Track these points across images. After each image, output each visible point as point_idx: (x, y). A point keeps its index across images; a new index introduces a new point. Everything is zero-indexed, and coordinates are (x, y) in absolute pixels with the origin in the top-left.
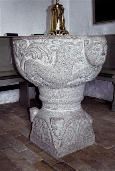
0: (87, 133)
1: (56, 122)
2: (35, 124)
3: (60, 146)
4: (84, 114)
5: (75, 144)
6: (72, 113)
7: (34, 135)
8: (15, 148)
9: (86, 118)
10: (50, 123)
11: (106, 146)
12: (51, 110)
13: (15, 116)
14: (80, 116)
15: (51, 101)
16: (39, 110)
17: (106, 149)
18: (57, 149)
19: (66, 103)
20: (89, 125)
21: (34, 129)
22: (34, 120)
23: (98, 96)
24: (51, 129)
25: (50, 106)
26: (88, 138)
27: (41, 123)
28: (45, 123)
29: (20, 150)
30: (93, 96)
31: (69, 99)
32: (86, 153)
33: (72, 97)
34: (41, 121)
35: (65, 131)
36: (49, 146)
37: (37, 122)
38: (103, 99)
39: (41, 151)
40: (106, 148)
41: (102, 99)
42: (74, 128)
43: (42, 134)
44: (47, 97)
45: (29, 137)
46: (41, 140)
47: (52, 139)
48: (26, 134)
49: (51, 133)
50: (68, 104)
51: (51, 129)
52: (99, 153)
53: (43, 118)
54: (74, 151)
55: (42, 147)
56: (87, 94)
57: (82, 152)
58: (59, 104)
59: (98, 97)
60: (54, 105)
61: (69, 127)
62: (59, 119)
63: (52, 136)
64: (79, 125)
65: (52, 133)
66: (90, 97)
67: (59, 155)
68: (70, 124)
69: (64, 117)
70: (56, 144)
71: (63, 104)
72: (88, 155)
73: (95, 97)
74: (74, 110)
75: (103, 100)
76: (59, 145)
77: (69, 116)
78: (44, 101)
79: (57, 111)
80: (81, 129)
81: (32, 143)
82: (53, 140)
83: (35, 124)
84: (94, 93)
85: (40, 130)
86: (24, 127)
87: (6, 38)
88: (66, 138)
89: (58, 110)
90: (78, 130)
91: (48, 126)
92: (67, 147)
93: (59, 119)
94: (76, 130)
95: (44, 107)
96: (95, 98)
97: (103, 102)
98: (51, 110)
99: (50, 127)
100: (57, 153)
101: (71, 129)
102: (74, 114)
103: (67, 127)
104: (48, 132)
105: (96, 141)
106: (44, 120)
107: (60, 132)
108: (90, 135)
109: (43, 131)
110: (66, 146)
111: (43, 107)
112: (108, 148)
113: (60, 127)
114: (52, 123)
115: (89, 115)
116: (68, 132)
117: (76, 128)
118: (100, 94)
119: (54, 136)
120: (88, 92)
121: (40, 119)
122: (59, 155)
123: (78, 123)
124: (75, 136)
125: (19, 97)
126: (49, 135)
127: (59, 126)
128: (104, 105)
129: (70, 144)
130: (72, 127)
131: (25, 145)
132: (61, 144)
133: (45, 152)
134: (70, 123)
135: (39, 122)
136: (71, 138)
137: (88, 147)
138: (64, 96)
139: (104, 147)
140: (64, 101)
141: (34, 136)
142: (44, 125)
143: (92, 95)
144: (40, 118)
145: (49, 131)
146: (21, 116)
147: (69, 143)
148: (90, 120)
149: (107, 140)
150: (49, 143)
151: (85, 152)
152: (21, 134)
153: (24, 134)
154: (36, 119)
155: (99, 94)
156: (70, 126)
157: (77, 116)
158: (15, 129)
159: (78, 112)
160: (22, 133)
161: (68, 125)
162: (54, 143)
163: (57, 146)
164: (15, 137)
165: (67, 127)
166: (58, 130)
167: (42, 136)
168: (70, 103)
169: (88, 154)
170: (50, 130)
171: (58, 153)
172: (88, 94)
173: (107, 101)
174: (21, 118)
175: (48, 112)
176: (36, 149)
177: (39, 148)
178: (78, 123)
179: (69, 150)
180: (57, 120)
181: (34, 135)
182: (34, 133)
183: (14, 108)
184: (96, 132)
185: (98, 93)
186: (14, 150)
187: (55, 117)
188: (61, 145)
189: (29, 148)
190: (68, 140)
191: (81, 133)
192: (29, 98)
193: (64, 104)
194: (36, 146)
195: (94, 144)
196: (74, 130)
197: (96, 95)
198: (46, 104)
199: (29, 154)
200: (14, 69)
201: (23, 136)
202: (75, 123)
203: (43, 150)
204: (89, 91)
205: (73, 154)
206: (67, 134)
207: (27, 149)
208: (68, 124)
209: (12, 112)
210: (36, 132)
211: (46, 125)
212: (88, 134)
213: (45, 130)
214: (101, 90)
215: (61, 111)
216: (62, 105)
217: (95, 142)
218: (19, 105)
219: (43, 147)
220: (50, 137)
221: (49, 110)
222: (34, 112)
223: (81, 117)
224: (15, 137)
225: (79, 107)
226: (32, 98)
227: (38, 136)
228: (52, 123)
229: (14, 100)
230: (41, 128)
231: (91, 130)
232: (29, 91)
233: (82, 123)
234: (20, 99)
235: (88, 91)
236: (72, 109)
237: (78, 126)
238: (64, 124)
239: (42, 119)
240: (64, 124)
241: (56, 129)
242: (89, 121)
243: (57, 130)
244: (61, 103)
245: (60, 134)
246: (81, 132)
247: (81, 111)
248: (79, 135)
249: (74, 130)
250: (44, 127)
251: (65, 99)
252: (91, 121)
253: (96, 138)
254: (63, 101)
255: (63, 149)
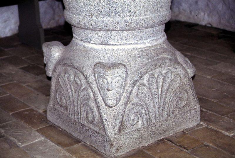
0: (181, 99)
1: (109, 72)
2: (58, 82)
3: (120, 131)
4: (174, 54)
5: (154, 124)
6: (144, 52)
7: (57, 107)
8: (12, 139)
9: (178, 63)
10: (93, 76)
11: (228, 130)
12: (95, 46)
13: (11, 68)
14: (163, 59)
15: (93, 23)
16: (64, 47)
17: (227, 136)
18: (113, 135)
19: (129, 28)
20: (186, 81)
21: (56, 92)
22: (54, 71)
23: (204, 19)
24: (96, 90)
25: (93, 35)
26: (183, 110)
27: (72, 76)
28: (82, 76)
29: (25, 142)
30: (192, 21)
31: (138, 18)
32: (180, 146)
33: (143, 13)
34: (71, 71)
35: (130, 93)
36: (94, 132)
37: (63, 75)
38: (215, 25)
39: (76, 143)
40: (227, 134)
41: (212, 28)
42: (150, 88)
43: (76, 104)
44: (84, 14)
45: (45, 112)
46: (73, 117)
47: (100, 113)
48: (37, 105)
49: (96, 100)
50: (134, 30)
51: (96, 90)
52: (211, 145)
53: (76, 65)
54: (152, 141)
55: (75, 134)
56: (177, 16)
57: (169, 143)
58: (112, 30)
59: (204, 23)
60: (102, 32)
61: (138, 84)
62: (115, 65)
63: (98, 107)
64: (163, 79)
65: (98, 100)
66: (186, 22)
67: (117, 150)
68: (141, 77)
69: (125, 62)
70: (110, 124)
71: (122, 30)
72: (185, 150)
73: (197, 22)
74: (148, 45)
75: (216, 28)
76: (117, 127)
77: (139, 60)
78: (76, 24)
79: (107, 47)
80: (168, 90)
81: (53, 127)
82: (101, 116)
83: (58, 82)
84: (193, 13)
85: (71, 95)
86: (33, 90)
87: (89, 153)
88: (133, 111)
89: (110, 45)
90: (160, 93)
91: (88, 83)
92: (134, 131)
93: (115, 65)
94: (155, 91)
95: (78, 35)
96: (196, 25)
97: (215, 33)
98: (95, 46)
99: (94, 85)
100: (112, 145)
101: (145, 90)
102: (150, 55)
103: (134, 85)
104: (89, 99)
105: (202, 118)
106: (79, 69)
107: (117, 96)
108: (187, 105)
109: (76, 96)
110: (133, 129)
111: (74, 39)
112: (232, 134)
113: (117, 85)
114: (100, 77)
115: (186, 56)
116: (137, 96)
117: (155, 87)
118: (208, 15)
119: (104, 105)
120: (179, 11)
121: (69, 68)
122: (117, 150)
123: (160, 76)
124: (154, 106)
125: (18, 24)
126: (93, 105)
127: (114, 81)
128: (219, 41)
129: (143, 124)
130: (145, 85)
131: (37, 131)
132: (122, 124)
133: (85, 146)
134: (140, 75)
135: (67, 75)
136: (143, 111)
137: (184, 133)
138: (123, 10)
139: (223, 132)
140: (126, 21)
141: (55, 109)
142: (79, 82)
143: (190, 18)
144: (68, 65)
145: (92, 95)
146: (25, 66)
147: (140, 123)
148: (187, 68)
149: (228, 117)
150: (92, 123)
151: (179, 142)
152: (26, 105)
153: (32, 107)
154: (60, 68)
155: (206, 15)
156: (140, 81)
157: (158, 60)
158: (10, 95)
159: (158, 51)
160: (27, 104)
161: (137, 81)
162: (105, 122)
163: (111, 131)
164: (11, 114)
165: (134, 85)
166: (114, 91)
167: (76, 108)
168: (140, 27)
169: (184, 148)
170: (94, 93)
171: (116, 145)
172: (180, 16)
173: (224, 31)
174: (26, 70)
175: (88, 50)
176: (62, 139)
177: (69, 136)
178: (160, 76)
179: (141, 139)
180: (110, 68)
181: (57, 107)
182: (56, 103)
183: (6, 50)
184: (201, 100)
185: (202, 14)
186: (11, 141)
187: (103, 61)
188: (120, 128)
189: (47, 137)
190: (137, 116)
191: (167, 100)
192: (41, 27)
193: (126, 30)
194: (63, 133)
195: (198, 125)
196: (151, 93)
197: (198, 18)
198: (81, 32)
199: (47, 150)
200: (42, 54)
201: (32, 110)
202: (153, 75)
203: (78, 141)
204: (181, 8)
205: (149, 147)
206: (135, 101)
207: (42, 138)
208: (137, 78)
209: (6, 57)
210: (61, 99)
211: (83, 81)
212: (184, 103)
213: (82, 94)
214: (210, 6)
215: (119, 47)
216: (120, 32)
217: (201, 120)
218: (20, 43)
219: (80, 132)
220: (95, 110)
221: (90, 45)
222: (53, 53)
223: (167, 61)
224: (11, 114)
225: (160, 38)
226: (49, 27)
227: (66, 108)
228: (98, 76)
229: (7, 30)
230: (73, 89)
231: (191, 93)
232: (42, 11)
233: (169, 75)
234: (20, 27)
235: (179, 8)
236: (145, 41)
237: (161, 84)
238: (127, 77)
239: (72, 66)
240: (127, 77)
241: (109, 90)
242: (187, 72)
243: (110, 93)
244: (118, 27)
245: (118, 101)
246: (167, 96)
247: (166, 47)
248: (162, 104)
249: (151, 93)
250: (78, 87)
251: (127, 19)
252: (191, 72)
253: (201, 111)
254: (122, 24)
255: (125, 137)
